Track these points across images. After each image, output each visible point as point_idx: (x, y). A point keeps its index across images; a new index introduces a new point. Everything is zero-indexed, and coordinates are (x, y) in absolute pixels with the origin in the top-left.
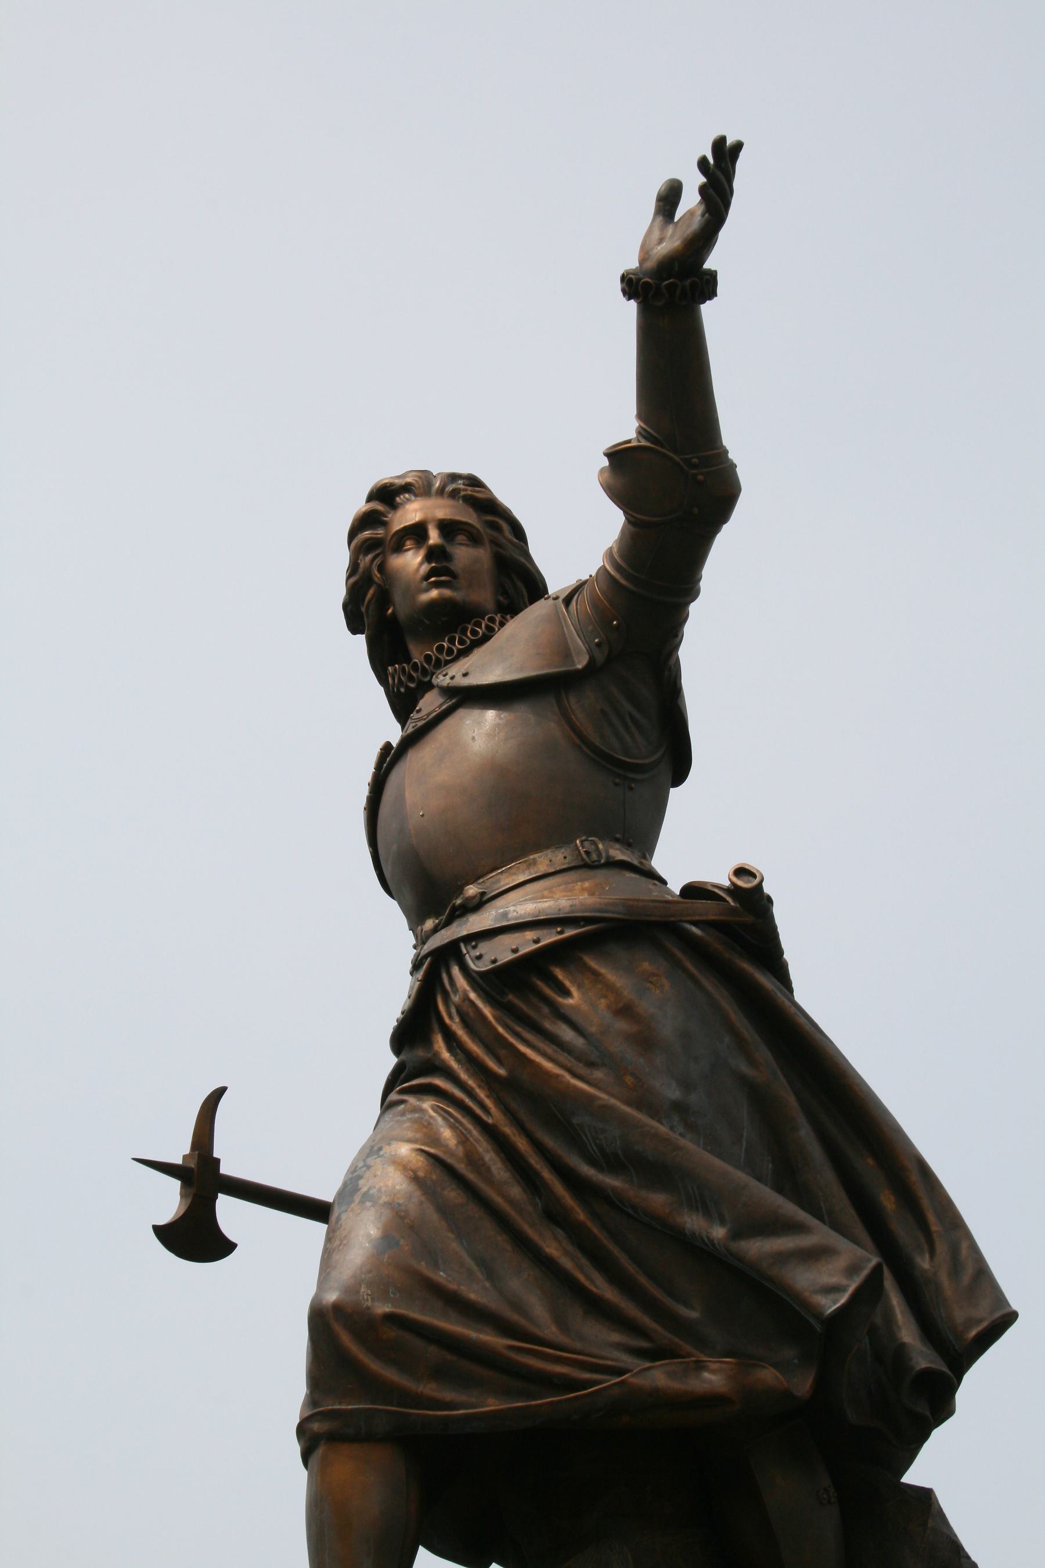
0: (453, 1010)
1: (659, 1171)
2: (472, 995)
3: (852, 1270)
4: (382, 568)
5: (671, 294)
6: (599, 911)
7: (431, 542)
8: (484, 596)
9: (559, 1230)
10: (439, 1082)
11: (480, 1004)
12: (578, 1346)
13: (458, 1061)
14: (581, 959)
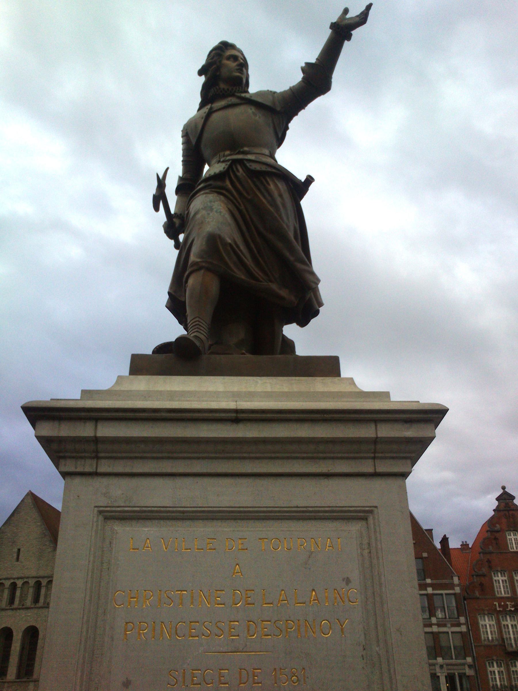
5: (342, 31)
10: (224, 192)
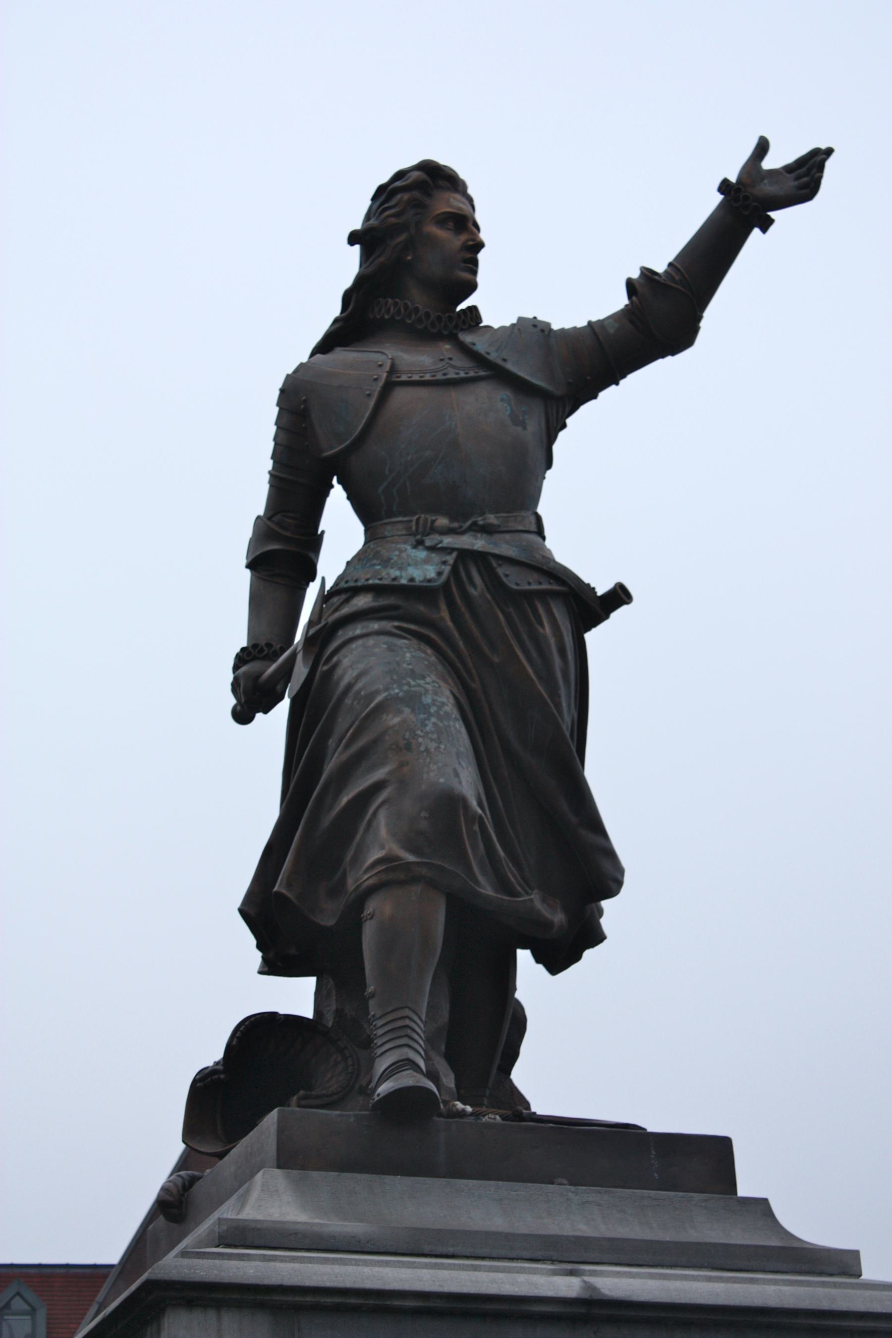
5: (753, 200)
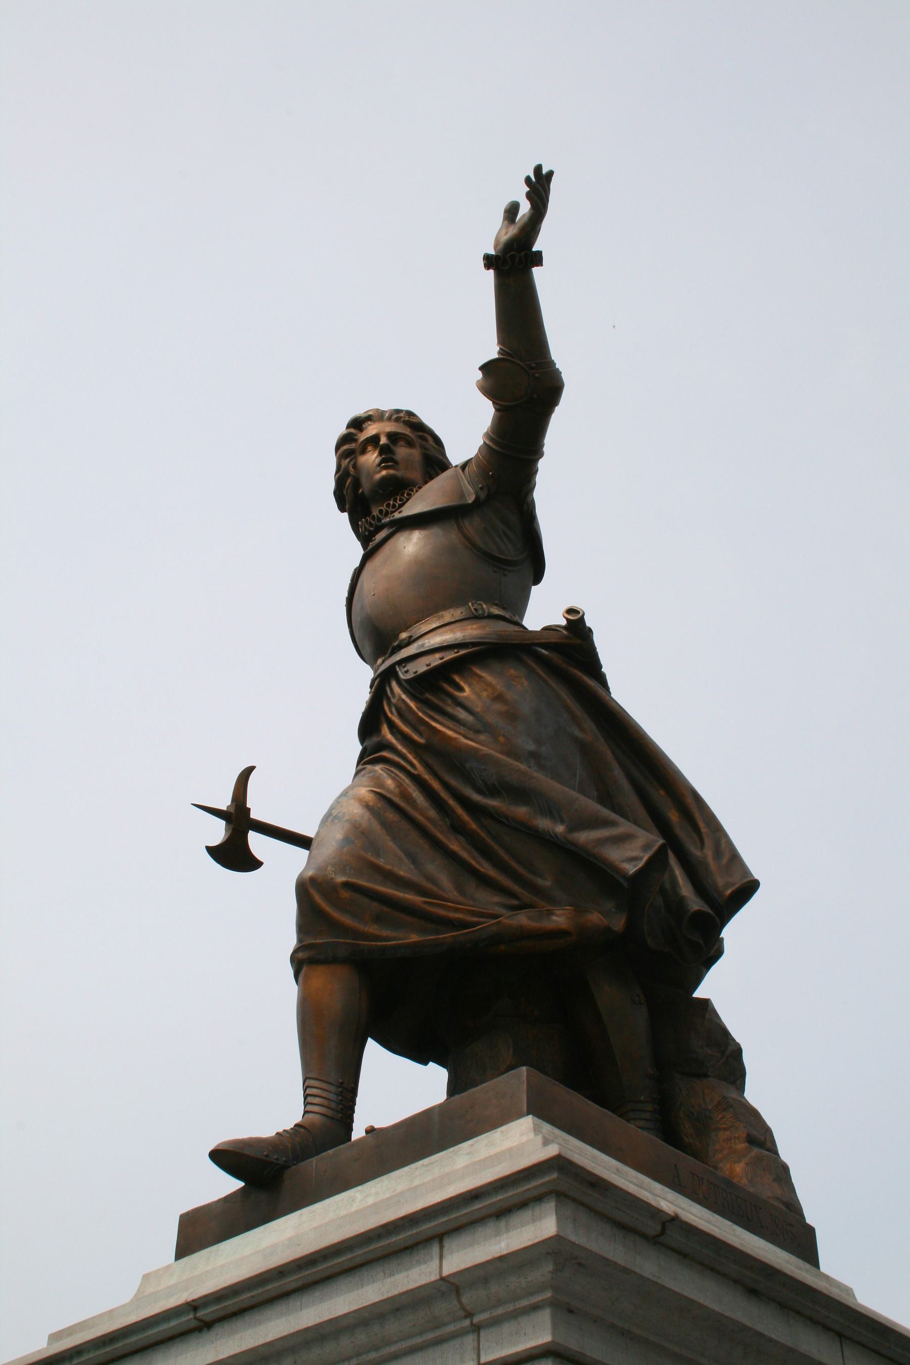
0: (394, 710)
1: (521, 793)
2: (404, 696)
3: (646, 848)
4: (355, 466)
5: (513, 264)
6: (482, 638)
7: (381, 443)
8: (415, 475)
9: (462, 838)
10: (385, 754)
11: (408, 701)
12: (471, 903)
13: (397, 739)
14: (471, 669)
